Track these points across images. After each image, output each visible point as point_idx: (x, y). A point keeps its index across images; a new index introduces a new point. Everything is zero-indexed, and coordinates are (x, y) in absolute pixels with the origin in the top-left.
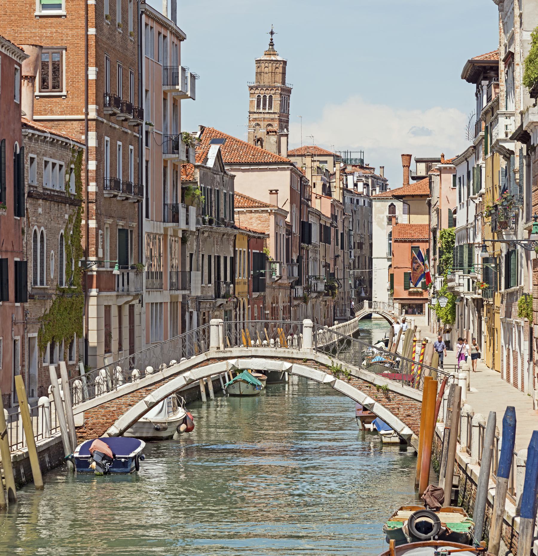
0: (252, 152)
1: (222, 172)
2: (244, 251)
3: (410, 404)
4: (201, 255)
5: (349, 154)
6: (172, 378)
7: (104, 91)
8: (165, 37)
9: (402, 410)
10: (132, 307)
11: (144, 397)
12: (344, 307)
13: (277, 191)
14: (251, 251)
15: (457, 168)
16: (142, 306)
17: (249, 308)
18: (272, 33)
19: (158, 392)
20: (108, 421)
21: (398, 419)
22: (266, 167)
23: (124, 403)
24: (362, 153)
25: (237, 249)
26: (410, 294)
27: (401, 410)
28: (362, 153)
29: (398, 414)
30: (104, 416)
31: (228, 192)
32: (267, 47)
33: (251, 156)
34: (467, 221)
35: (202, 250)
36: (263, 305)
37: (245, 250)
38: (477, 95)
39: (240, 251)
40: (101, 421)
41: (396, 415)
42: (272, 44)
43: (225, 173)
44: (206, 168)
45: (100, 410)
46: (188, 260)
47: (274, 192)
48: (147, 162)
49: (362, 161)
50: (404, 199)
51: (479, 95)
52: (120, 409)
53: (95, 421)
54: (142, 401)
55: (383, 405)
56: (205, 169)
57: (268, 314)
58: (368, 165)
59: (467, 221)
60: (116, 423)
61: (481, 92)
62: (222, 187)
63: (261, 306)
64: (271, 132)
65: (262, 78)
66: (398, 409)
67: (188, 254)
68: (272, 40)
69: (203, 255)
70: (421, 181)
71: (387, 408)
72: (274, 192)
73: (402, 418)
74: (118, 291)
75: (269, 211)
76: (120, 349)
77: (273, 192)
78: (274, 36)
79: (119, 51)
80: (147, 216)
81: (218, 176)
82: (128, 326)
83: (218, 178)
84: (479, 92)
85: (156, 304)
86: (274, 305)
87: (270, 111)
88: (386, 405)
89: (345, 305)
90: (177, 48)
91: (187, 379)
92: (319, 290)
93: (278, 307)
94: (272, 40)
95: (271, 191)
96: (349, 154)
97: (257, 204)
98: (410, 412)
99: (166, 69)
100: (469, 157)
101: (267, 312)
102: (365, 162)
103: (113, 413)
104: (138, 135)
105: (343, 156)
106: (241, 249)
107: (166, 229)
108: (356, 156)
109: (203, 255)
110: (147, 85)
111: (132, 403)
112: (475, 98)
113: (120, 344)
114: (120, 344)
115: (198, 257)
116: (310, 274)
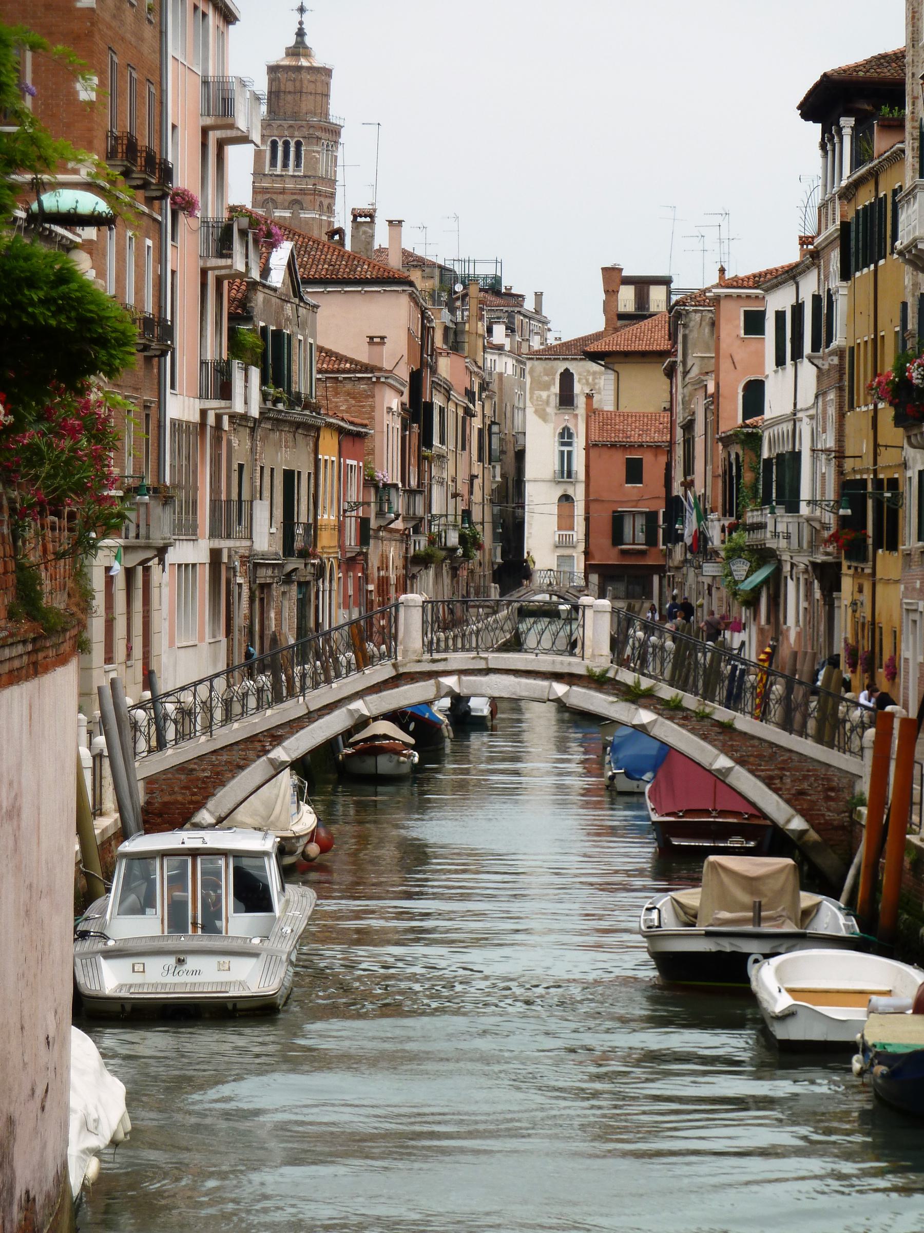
0: (329, 257)
1: (295, 296)
2: (333, 462)
3: (806, 769)
4: (259, 468)
5: (472, 265)
6: (323, 712)
7: (125, 127)
8: (204, 15)
9: (789, 780)
10: (147, 570)
11: (269, 751)
12: (482, 580)
13: (382, 338)
14: (345, 461)
15: (767, 298)
16: (163, 570)
17: (339, 578)
18: (302, 10)
19: (297, 739)
20: (193, 798)
21: (780, 800)
22: (360, 289)
23: (228, 763)
24: (499, 265)
25: (320, 457)
26: (624, 553)
27: (788, 781)
28: (499, 265)
29: (780, 789)
30: (187, 788)
31: (305, 340)
32: (291, 41)
33: (326, 266)
34: (795, 405)
35: (261, 459)
36: (363, 573)
37: (334, 459)
38: (823, 146)
39: (326, 461)
40: (180, 798)
41: (776, 791)
42: (301, 33)
43: (301, 299)
44: (269, 288)
45: (177, 776)
46: (235, 476)
47: (378, 340)
48: (173, 272)
49: (497, 280)
50: (607, 360)
51: (829, 147)
52: (218, 774)
53: (167, 798)
54: (264, 758)
55: (751, 772)
56: (267, 291)
57: (371, 591)
58: (511, 289)
59: (795, 405)
60: (211, 804)
61: (836, 140)
62: (295, 329)
63: (360, 575)
64: (361, 216)
65: (282, 103)
66: (781, 778)
67: (236, 467)
68: (301, 23)
69: (262, 468)
70: (642, 323)
71: (757, 777)
72: (376, 341)
73: (788, 796)
74: (127, 538)
75: (374, 379)
76: (129, 656)
77: (375, 340)
78: (306, 17)
79: (130, 43)
80: (173, 387)
81: (289, 305)
82: (103, 613)
83: (288, 309)
84: (831, 140)
85: (187, 565)
86: (382, 573)
87: (296, 174)
88: (757, 770)
89: (484, 576)
90: (222, 36)
91: (356, 716)
92: (449, 544)
93: (388, 578)
94: (301, 23)
95: (371, 338)
96: (472, 265)
97: (348, 365)
98: (805, 786)
99: (205, 83)
100: (800, 274)
101: (371, 587)
102: (505, 283)
103: (204, 782)
104: (160, 218)
105: (458, 269)
106: (326, 457)
107: (204, 413)
108: (484, 270)
109: (262, 468)
110: (176, 114)
111: (242, 763)
112: (819, 152)
113: (129, 649)
114: (129, 649)
115: (253, 471)
116: (434, 512)
